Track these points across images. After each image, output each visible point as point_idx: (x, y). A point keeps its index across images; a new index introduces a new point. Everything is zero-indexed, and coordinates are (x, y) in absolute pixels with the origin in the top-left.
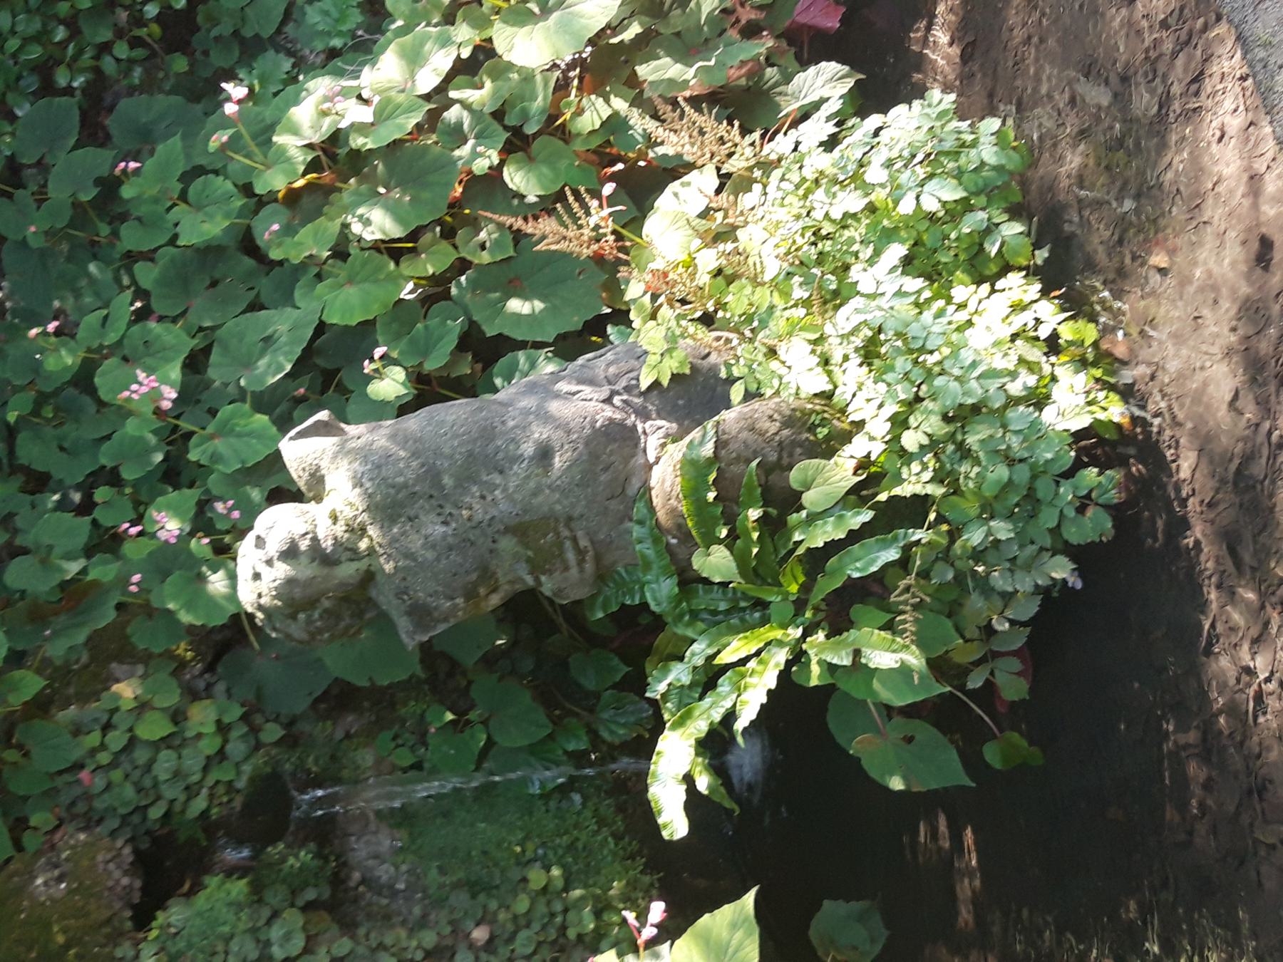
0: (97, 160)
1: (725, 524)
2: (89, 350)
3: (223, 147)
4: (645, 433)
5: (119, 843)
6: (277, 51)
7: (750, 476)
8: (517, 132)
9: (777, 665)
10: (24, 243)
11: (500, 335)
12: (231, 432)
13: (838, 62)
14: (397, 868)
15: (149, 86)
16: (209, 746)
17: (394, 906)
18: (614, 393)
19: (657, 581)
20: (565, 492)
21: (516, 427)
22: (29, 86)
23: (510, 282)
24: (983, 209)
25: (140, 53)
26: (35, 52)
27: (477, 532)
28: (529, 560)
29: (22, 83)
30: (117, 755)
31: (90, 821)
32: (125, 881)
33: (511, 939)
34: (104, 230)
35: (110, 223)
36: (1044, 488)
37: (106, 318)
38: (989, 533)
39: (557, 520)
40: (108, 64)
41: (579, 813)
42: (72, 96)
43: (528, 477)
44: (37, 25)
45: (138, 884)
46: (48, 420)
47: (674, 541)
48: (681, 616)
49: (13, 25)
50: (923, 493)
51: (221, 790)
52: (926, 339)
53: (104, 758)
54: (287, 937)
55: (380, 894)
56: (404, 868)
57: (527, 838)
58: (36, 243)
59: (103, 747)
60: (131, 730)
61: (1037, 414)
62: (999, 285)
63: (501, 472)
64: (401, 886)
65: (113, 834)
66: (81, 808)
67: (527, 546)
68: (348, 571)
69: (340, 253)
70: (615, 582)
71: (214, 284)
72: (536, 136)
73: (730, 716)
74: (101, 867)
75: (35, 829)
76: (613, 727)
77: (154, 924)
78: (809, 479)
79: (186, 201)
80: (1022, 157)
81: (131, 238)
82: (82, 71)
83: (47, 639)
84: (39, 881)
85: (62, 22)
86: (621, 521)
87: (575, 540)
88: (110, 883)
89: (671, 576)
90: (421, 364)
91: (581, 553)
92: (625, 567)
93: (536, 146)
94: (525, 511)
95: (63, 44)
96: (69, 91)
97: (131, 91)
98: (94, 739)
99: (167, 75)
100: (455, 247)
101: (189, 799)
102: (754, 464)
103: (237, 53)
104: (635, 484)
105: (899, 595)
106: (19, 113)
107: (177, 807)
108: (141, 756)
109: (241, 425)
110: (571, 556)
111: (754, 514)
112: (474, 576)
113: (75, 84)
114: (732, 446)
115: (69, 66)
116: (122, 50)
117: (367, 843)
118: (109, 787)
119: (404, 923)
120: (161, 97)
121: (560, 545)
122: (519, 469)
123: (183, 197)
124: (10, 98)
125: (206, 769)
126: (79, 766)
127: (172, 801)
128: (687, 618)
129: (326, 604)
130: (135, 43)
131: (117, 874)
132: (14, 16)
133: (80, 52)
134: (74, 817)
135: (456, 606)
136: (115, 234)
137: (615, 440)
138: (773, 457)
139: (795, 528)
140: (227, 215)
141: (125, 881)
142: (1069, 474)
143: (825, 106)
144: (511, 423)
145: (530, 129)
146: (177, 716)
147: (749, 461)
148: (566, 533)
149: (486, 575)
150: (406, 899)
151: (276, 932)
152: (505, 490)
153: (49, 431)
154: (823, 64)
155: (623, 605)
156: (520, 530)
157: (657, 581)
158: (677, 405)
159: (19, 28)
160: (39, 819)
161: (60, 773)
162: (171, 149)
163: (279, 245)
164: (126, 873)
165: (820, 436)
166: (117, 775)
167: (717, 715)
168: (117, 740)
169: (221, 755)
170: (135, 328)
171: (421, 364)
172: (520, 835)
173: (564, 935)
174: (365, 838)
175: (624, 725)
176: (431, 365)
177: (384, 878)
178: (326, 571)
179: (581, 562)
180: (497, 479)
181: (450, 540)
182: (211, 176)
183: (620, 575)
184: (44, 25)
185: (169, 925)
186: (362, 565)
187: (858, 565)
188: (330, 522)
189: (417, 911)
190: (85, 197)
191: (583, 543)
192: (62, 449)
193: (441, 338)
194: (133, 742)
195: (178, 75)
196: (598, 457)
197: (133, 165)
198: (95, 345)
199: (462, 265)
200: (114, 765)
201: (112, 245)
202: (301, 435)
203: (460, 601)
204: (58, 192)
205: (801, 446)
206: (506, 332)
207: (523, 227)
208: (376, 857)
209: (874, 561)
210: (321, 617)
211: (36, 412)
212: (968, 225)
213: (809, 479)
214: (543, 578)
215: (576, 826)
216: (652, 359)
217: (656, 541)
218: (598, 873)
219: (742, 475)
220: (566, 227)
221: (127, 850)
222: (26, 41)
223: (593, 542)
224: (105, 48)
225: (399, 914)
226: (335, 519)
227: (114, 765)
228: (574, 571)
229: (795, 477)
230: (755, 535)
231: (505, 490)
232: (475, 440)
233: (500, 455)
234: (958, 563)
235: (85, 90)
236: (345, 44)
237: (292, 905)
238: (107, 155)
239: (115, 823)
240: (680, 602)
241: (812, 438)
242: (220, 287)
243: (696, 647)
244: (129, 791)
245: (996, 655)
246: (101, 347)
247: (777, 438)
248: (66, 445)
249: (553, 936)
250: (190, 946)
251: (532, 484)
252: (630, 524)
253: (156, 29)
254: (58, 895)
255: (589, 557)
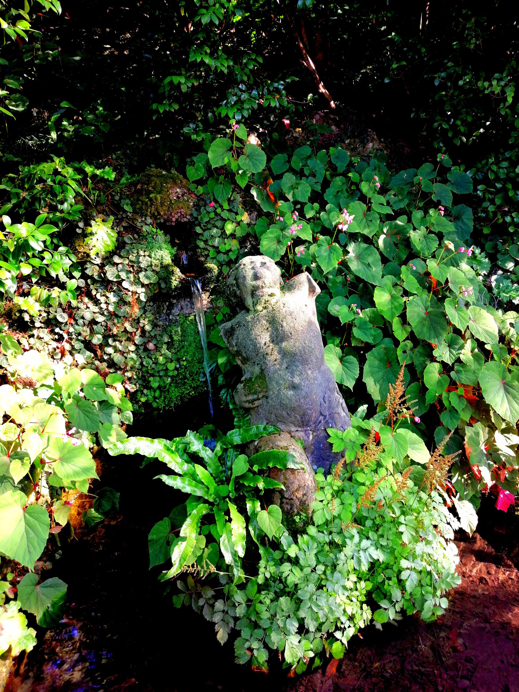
0: (448, 201)
1: (259, 470)
2: (370, 199)
3: (446, 247)
4: (306, 431)
5: (188, 217)
6: (491, 268)
7: (277, 484)
8: (452, 368)
9: (195, 491)
10: (416, 175)
11: (366, 359)
12: (331, 252)
13: (478, 525)
14: (178, 315)
15: (477, 219)
16: (223, 248)
17: (162, 315)
18: (325, 417)
19: (240, 435)
20: (277, 396)
21: (308, 375)
22: (478, 176)
23: (390, 363)
24: (403, 597)
25: (491, 215)
26: (491, 176)
27: (262, 357)
28: (251, 379)
29: (479, 173)
30: (220, 215)
31: (197, 207)
32: (174, 219)
33: (149, 357)
34: (421, 205)
35: (423, 206)
36: (259, 633)
37: (383, 204)
38: (240, 604)
39: (266, 392)
40: (486, 204)
41: (198, 380)
42: (474, 191)
43: (284, 380)
44: (502, 176)
45: (174, 224)
46: (350, 187)
47: (256, 444)
48: (225, 444)
49: (503, 168)
50: (260, 573)
51: (206, 253)
52: (331, 581)
53: (219, 210)
54: (147, 277)
55: (168, 309)
56: (178, 318)
57: (189, 362)
58: (416, 180)
59: (223, 210)
60: (229, 219)
61: (294, 633)
62: (365, 606)
63: (287, 368)
64: (171, 317)
65: (191, 215)
66: (201, 203)
67: (256, 378)
68: (249, 302)
69: (406, 293)
70: (244, 414)
71: (396, 245)
72: (449, 376)
73: (170, 472)
74: (179, 211)
75: (197, 188)
76: (225, 394)
77: (158, 230)
78: (273, 514)
79: (429, 233)
80: (429, 618)
81: (418, 215)
82: (484, 194)
83: (258, 188)
84: (178, 190)
85: (504, 186)
86: (267, 419)
87: (258, 399)
88: (173, 214)
89: (241, 441)
90: (356, 326)
91: (252, 401)
92: (250, 419)
93: (445, 376)
94: (270, 378)
95: (495, 187)
96: (475, 190)
97: (475, 213)
98: (226, 206)
99: (482, 226)
100: (404, 341)
101: (204, 241)
102: (283, 487)
103: (491, 252)
104: (282, 427)
105: (206, 562)
106: (468, 173)
107: (200, 237)
108: (219, 224)
109: (334, 256)
110: (250, 398)
111: (261, 485)
112: (244, 355)
113: (478, 192)
114: (292, 477)
115: (486, 190)
116: (491, 208)
117: (187, 305)
118: (209, 213)
119: (156, 318)
120: (473, 224)
121: (255, 393)
122: (288, 376)
123: (431, 232)
124: (474, 169)
125: (213, 247)
126: (216, 202)
127: (203, 235)
128: (225, 447)
129: (238, 292)
130: (495, 213)
131: (176, 216)
132: (506, 168)
133: (491, 193)
134: (199, 201)
135: (234, 346)
136: (420, 208)
137: (302, 418)
138: (286, 495)
139: (253, 504)
140: (422, 249)
141: (174, 219)
142: (266, 646)
143: (456, 519)
144: (309, 372)
145: (453, 374)
146: (233, 236)
147: (284, 484)
148: (260, 396)
149: (245, 360)
150: (166, 319)
151: (149, 273)
152: (280, 370)
153: (345, 188)
154: (476, 517)
155: (234, 417)
156: (262, 375)
157: (240, 435)
158: (320, 444)
159: (501, 170)
160: (201, 189)
161: (214, 195)
162: (449, 227)
163: (407, 270)
164: (177, 220)
165: (295, 518)
166: (212, 215)
167: (172, 465)
168: (225, 215)
169: (219, 252)
170: (378, 216)
171: (356, 326)
172: (190, 359)
173: (151, 376)
174: (189, 304)
175: (226, 398)
176: (355, 331)
177: (173, 311)
178: (250, 292)
179: (248, 402)
180: (284, 366)
181: (258, 345)
182: (438, 243)
183: (247, 416)
184: (502, 179)
185: (157, 235)
186: (251, 308)
187: (226, 541)
188: (270, 293)
189: (161, 323)
190: (433, 197)
191: (257, 403)
192: (338, 192)
193: (366, 334)
194: (224, 220)
195: (482, 230)
196: (293, 411)
197: (443, 213)
198: (372, 201)
199: (397, 343)
200: (216, 214)
201: (416, 208)
202: (309, 280)
203: (235, 349)
204: (436, 187)
205: (291, 509)
206: (367, 362)
207: (399, 380)
208: (182, 308)
209: (226, 549)
210: (234, 290)
211: (353, 183)
212: (396, 594)
213: (273, 514)
214: (242, 385)
215: (193, 379)
216: (340, 433)
217: (257, 435)
218: (176, 387)
219: (279, 480)
220: (400, 398)
221: (185, 220)
222: (496, 174)
223: (258, 406)
224: (492, 202)
225: (160, 317)
226: (271, 295)
227: (216, 214)
228: (244, 399)
229: (275, 508)
230: (252, 485)
231: (280, 370)
232: (301, 356)
233: (294, 368)
234: (227, 586)
235: (477, 196)
236: (494, 294)
237: (160, 279)
238: (449, 205)
239: (195, 215)
240: (231, 444)
241: (294, 514)
242: (394, 247)
243: (209, 452)
244: (206, 219)
245: (191, 595)
246: (371, 203)
247: (295, 498)
248: (339, 194)
249: (150, 372)
250: (149, 243)
251: (281, 382)
252: (265, 424)
253: (501, 221)
254: (171, 196)
255: (251, 405)
